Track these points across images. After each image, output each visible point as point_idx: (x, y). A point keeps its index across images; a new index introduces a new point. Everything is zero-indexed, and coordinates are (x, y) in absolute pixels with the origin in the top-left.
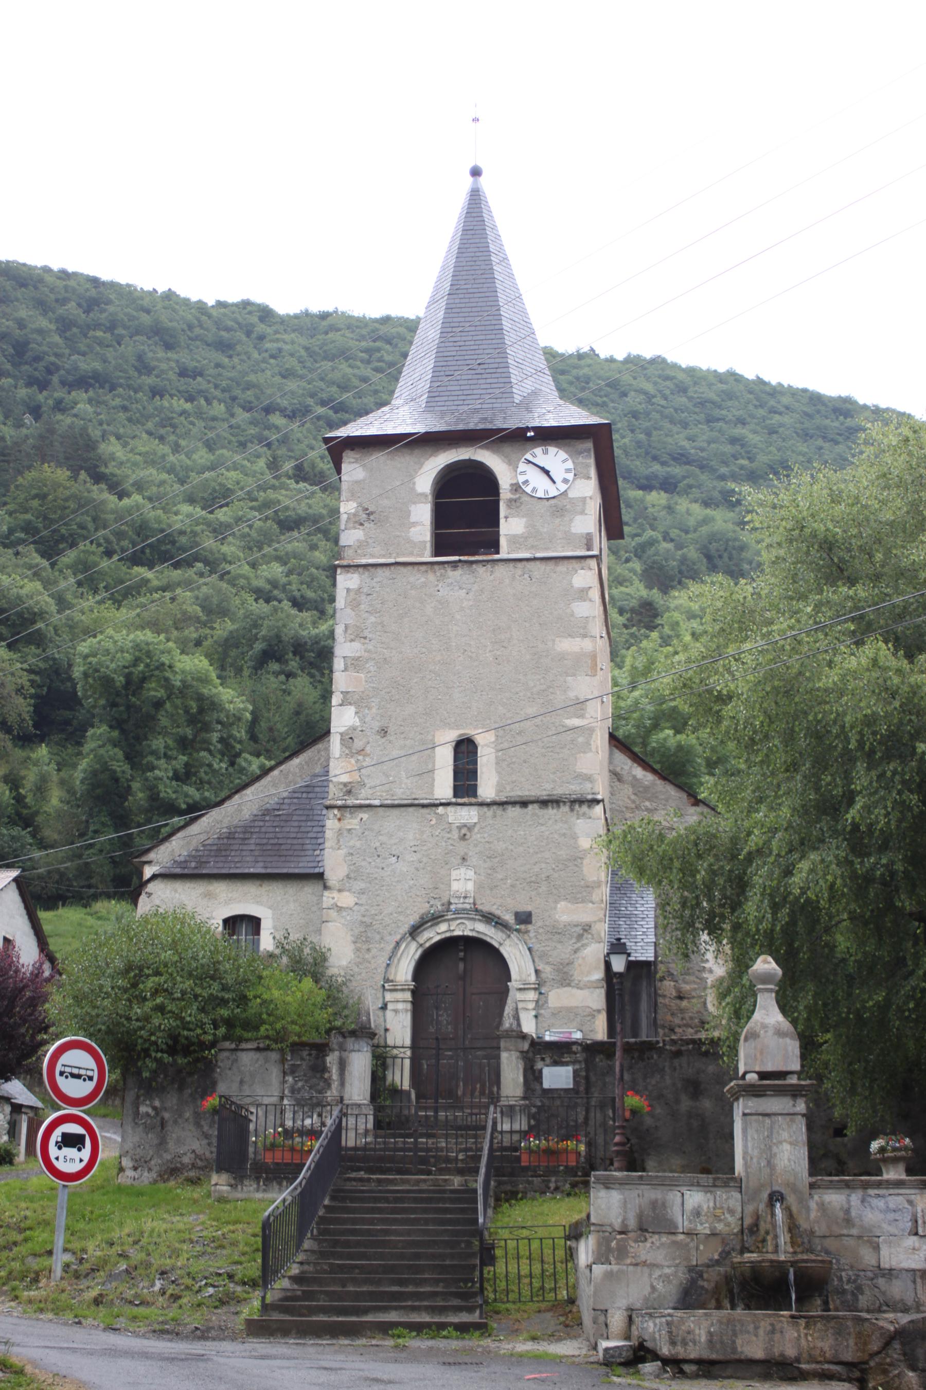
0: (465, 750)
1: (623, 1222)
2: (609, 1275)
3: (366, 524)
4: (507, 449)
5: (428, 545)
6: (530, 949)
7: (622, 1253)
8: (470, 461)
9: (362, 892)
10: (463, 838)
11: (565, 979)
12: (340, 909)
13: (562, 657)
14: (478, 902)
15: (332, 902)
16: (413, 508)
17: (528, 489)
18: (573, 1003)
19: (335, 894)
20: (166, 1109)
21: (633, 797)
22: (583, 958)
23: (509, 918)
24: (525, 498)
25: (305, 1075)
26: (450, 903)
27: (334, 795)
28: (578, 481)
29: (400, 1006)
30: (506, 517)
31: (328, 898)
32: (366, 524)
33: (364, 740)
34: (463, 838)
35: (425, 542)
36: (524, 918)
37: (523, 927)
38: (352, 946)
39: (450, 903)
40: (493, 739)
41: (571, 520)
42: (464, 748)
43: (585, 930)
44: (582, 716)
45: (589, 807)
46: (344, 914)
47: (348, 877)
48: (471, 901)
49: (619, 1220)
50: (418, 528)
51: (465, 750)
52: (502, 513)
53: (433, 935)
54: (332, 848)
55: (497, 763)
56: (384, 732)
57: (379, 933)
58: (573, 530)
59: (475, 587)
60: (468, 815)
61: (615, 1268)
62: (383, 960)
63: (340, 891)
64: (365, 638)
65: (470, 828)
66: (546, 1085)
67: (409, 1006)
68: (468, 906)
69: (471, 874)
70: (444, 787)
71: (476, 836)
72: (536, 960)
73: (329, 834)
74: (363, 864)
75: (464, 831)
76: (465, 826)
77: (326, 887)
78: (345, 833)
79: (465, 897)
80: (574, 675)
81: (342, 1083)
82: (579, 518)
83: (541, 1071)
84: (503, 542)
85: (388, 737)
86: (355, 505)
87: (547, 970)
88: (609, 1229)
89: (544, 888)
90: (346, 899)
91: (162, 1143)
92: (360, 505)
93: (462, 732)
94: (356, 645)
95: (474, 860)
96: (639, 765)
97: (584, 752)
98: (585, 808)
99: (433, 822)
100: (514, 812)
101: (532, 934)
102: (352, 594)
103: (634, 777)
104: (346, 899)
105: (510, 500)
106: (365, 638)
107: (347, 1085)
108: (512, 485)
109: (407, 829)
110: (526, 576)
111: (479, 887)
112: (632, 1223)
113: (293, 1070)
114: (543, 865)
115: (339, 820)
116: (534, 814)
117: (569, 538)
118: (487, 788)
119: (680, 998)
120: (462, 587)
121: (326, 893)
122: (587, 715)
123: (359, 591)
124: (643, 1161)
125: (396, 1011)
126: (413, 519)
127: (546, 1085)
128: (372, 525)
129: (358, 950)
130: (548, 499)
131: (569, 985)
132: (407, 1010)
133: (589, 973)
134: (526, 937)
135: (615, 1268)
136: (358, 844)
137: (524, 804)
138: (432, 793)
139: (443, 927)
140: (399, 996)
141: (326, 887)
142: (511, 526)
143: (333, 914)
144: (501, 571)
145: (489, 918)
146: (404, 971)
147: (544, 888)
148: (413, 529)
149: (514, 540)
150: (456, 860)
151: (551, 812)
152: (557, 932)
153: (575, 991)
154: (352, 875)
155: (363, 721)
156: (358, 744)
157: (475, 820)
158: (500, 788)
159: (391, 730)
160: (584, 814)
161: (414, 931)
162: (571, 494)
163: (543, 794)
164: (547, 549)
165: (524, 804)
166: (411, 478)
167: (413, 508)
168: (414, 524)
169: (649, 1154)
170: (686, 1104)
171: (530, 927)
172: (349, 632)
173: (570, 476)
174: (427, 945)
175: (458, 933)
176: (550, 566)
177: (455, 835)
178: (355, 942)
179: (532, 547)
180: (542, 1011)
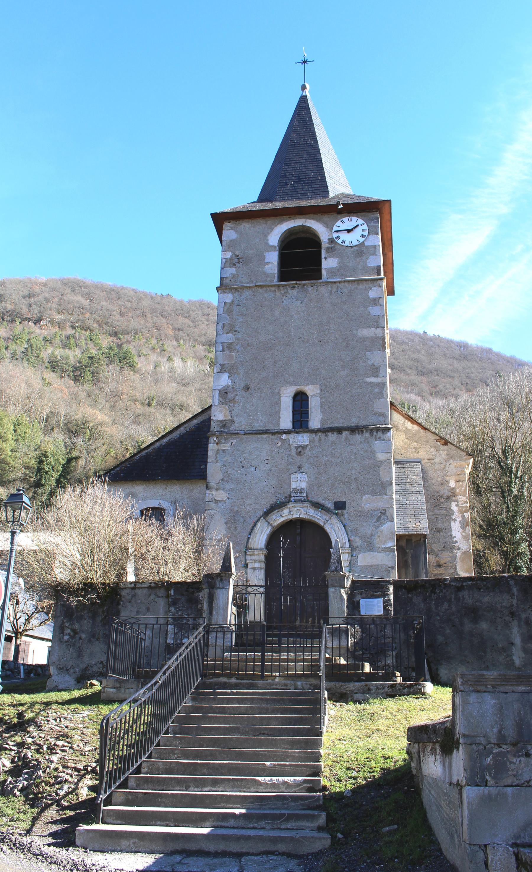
0: (300, 400)
1: (500, 731)
2: (487, 801)
3: (237, 265)
4: (326, 218)
5: (276, 276)
6: (344, 526)
7: (500, 768)
8: (303, 226)
9: (231, 490)
10: (299, 454)
11: (370, 546)
12: (217, 501)
13: (363, 340)
14: (310, 496)
15: (211, 496)
16: (266, 254)
17: (339, 241)
18: (375, 562)
19: (214, 492)
20: (83, 631)
21: (406, 440)
22: (381, 532)
23: (330, 505)
24: (337, 247)
25: (183, 607)
26: (290, 497)
27: (214, 427)
28: (371, 236)
29: (257, 565)
30: (326, 258)
31: (210, 494)
32: (237, 265)
33: (234, 393)
34: (299, 454)
35: (274, 274)
36: (340, 506)
37: (340, 511)
38: (224, 526)
39: (290, 497)
40: (319, 391)
41: (367, 259)
42: (299, 398)
43: (383, 514)
44: (377, 376)
45: (383, 433)
46: (220, 504)
47: (222, 480)
48: (305, 494)
49: (495, 730)
50: (270, 266)
51: (300, 400)
52: (323, 256)
53: (280, 518)
54: (212, 462)
55: (321, 406)
56: (247, 388)
57: (243, 517)
58: (369, 265)
59: (306, 300)
60: (302, 439)
61: (494, 791)
62: (245, 534)
63: (217, 490)
64: (236, 331)
65: (304, 448)
66: (363, 612)
67: (263, 565)
68: (303, 498)
69: (304, 476)
70: (286, 421)
71: (307, 452)
72: (349, 533)
73: (210, 453)
74: (232, 472)
75: (299, 450)
76: (301, 446)
77: (208, 487)
78: (221, 452)
79: (301, 492)
80: (371, 350)
81: (211, 613)
82: (372, 258)
83: (359, 603)
84: (324, 272)
85: (250, 391)
86: (230, 254)
87: (358, 542)
88: (482, 740)
89: (354, 486)
90: (221, 495)
91: (80, 655)
92: (233, 253)
93: (298, 387)
94: (230, 335)
95: (306, 467)
96: (409, 420)
97: (379, 398)
98: (380, 434)
99: (279, 444)
100: (333, 437)
101: (346, 516)
102: (228, 306)
103: (406, 428)
104: (221, 495)
105: (328, 248)
106: (236, 331)
107: (214, 613)
108: (329, 239)
109: (260, 450)
110: (339, 292)
111: (310, 485)
112: (511, 733)
113: (174, 603)
114: (353, 471)
115: (217, 444)
116: (346, 438)
117: (367, 270)
118: (315, 422)
119: (439, 566)
120: (297, 300)
121: (208, 492)
122: (380, 375)
123: (232, 303)
124: (437, 669)
125: (254, 569)
126: (267, 260)
127: (363, 612)
128: (241, 265)
129: (228, 528)
130: (352, 247)
131: (372, 550)
132: (261, 568)
133: (385, 542)
134: (342, 517)
135: (494, 791)
136: (229, 459)
137: (339, 430)
138: (279, 425)
139: (286, 511)
140: (256, 558)
141: (208, 487)
142: (328, 263)
143: (212, 505)
144: (324, 290)
145: (317, 506)
146: (260, 538)
147: (354, 486)
148: (266, 266)
149: (330, 271)
150: (294, 468)
151: (358, 437)
152: (363, 515)
153: (376, 553)
154: (225, 479)
155: (234, 382)
156: (230, 396)
157: (307, 443)
158: (323, 421)
159: (252, 386)
160: (380, 438)
161: (267, 514)
162: (366, 244)
163: (354, 422)
164: (352, 276)
165: (339, 430)
166: (266, 236)
167: (266, 254)
168: (267, 264)
169: (441, 664)
170: (468, 626)
171: (345, 512)
172: (226, 327)
173: (366, 233)
174: (275, 524)
175: (296, 516)
176: (355, 286)
177: (294, 451)
178: (226, 523)
179: (342, 275)
180: (354, 568)
